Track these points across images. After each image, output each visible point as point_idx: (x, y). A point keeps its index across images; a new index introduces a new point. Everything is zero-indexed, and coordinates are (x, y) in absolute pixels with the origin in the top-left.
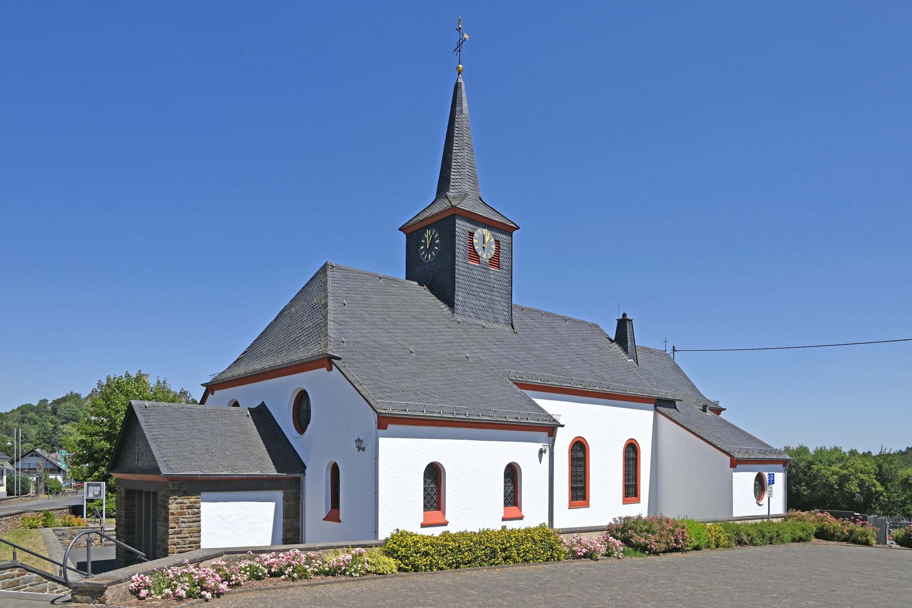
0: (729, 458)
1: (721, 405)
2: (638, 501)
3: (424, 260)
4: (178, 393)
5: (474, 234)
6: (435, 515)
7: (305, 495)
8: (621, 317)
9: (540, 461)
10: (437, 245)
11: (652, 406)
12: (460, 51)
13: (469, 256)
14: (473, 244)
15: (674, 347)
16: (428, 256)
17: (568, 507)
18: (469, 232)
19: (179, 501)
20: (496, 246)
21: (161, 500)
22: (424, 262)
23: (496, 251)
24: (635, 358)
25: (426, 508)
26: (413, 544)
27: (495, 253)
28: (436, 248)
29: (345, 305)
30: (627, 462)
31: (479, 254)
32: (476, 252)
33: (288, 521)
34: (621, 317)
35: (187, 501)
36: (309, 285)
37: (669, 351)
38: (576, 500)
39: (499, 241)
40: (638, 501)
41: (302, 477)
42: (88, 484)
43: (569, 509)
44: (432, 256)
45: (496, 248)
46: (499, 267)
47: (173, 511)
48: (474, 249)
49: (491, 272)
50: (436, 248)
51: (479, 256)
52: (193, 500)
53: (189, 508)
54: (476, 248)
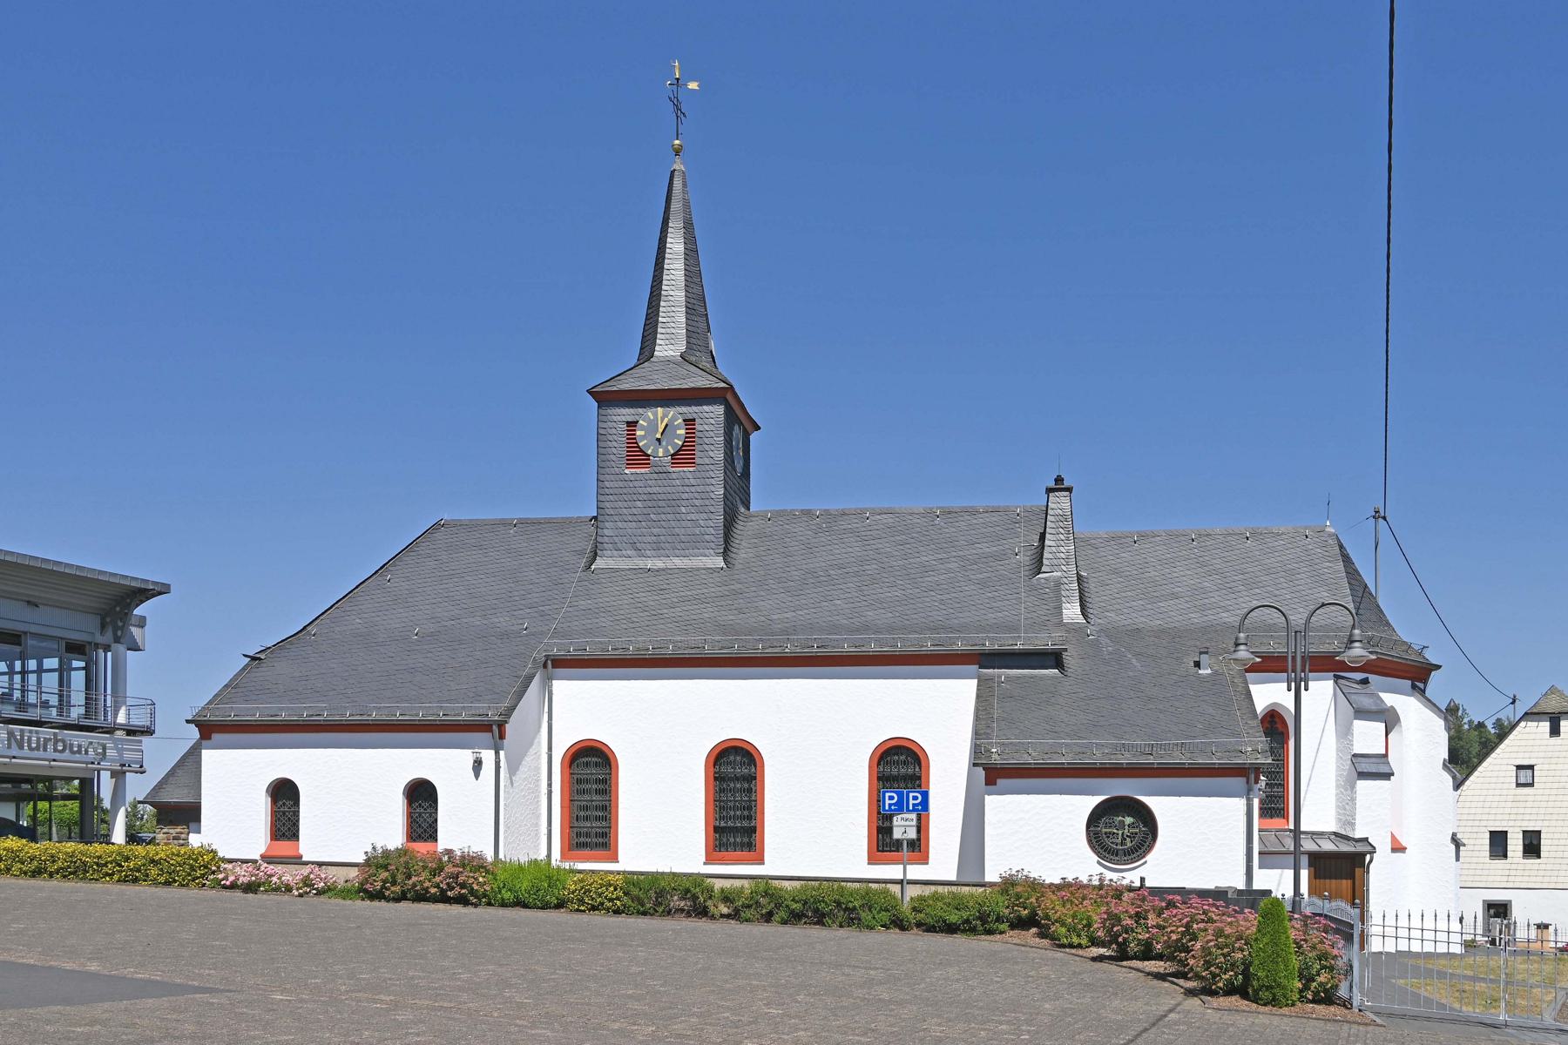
1: (1432, 657)
2: (872, 860)
4: (1476, 723)
6: (284, 848)
7: (1368, 902)
9: (477, 775)
13: (628, 460)
17: (704, 860)
18: (628, 422)
19: (164, 831)
25: (271, 840)
26: (1478, 1001)
29: (1193, 541)
31: (649, 452)
32: (641, 451)
35: (174, 831)
38: (735, 851)
40: (872, 860)
42: (924, 859)
43: (705, 864)
49: (674, 476)
51: (649, 456)
52: (178, 830)
53: (174, 838)
54: (640, 444)
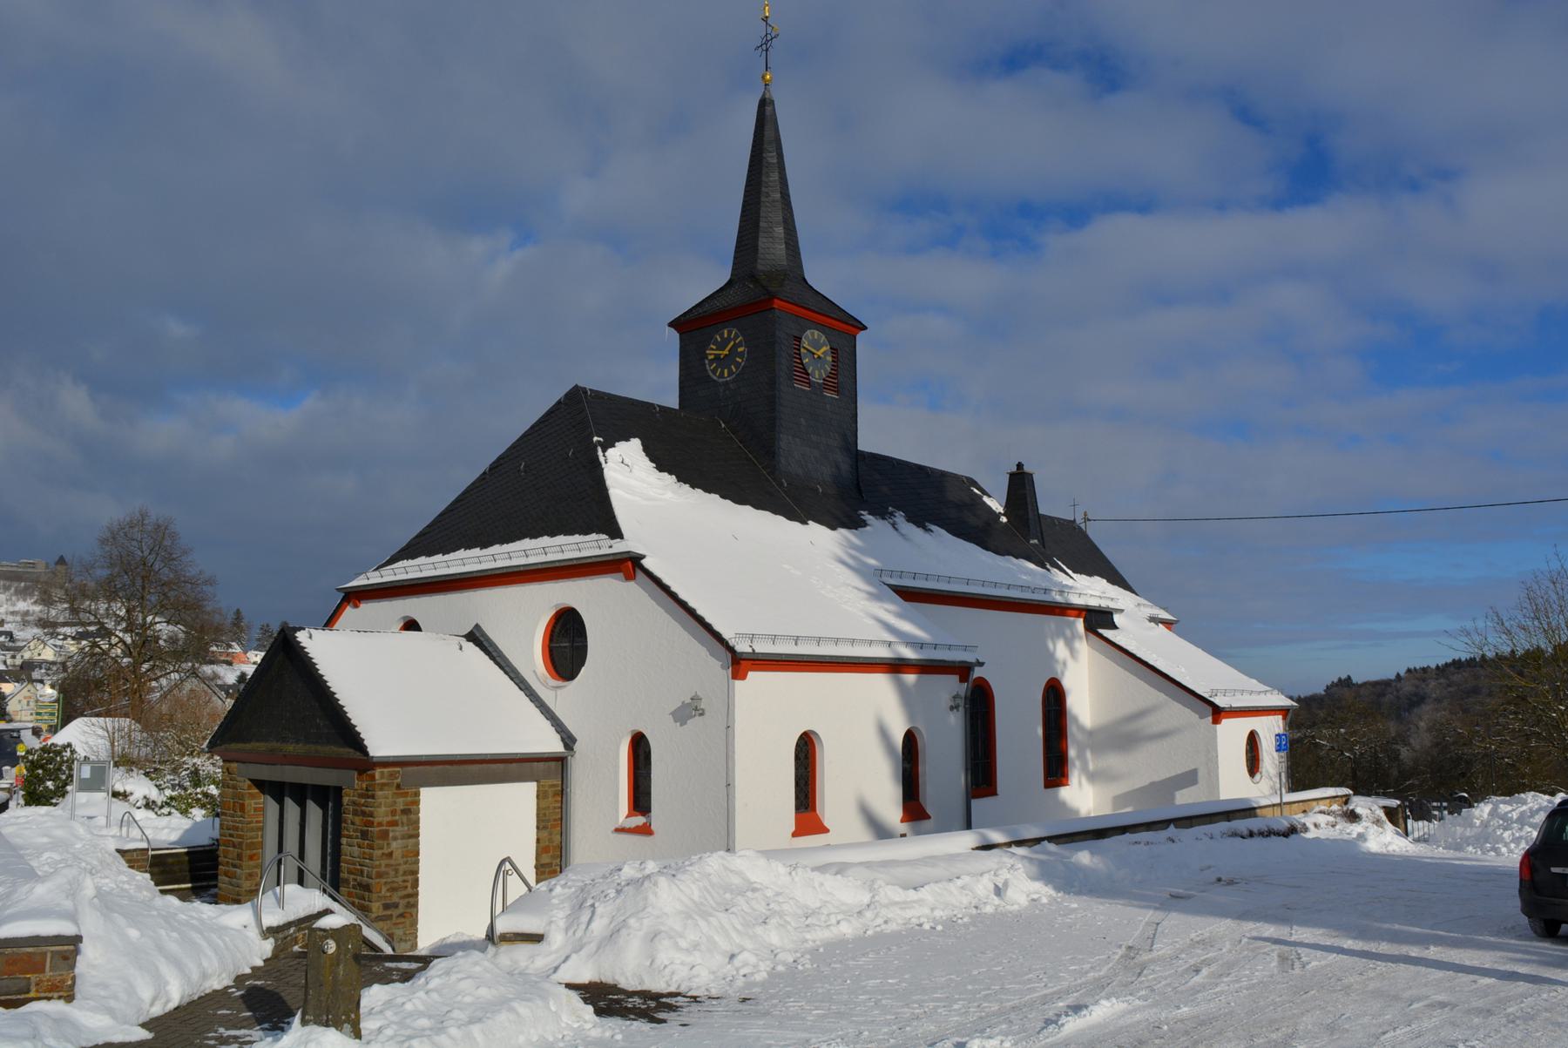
0: (1211, 709)
3: (715, 378)
5: (801, 339)
8: (1014, 469)
10: (741, 355)
11: (346, 604)
12: (767, 50)
14: (800, 355)
15: (1085, 514)
16: (722, 373)
20: (833, 357)
21: (354, 803)
22: (715, 381)
23: (833, 365)
24: (1040, 538)
27: (832, 369)
28: (739, 360)
30: (32, 995)
31: (810, 371)
32: (804, 369)
33: (545, 834)
34: (1014, 469)
36: (546, 423)
37: (1079, 520)
39: (836, 350)
41: (569, 758)
44: (730, 373)
45: (833, 361)
46: (837, 392)
47: (380, 819)
48: (802, 364)
50: (739, 360)
51: (808, 374)
